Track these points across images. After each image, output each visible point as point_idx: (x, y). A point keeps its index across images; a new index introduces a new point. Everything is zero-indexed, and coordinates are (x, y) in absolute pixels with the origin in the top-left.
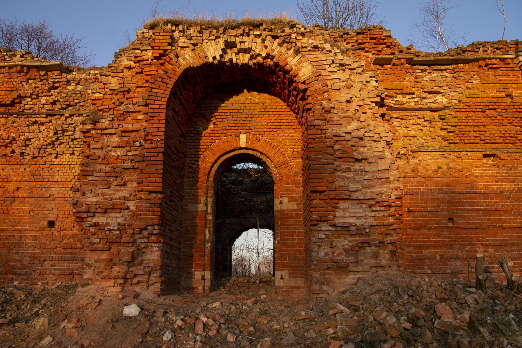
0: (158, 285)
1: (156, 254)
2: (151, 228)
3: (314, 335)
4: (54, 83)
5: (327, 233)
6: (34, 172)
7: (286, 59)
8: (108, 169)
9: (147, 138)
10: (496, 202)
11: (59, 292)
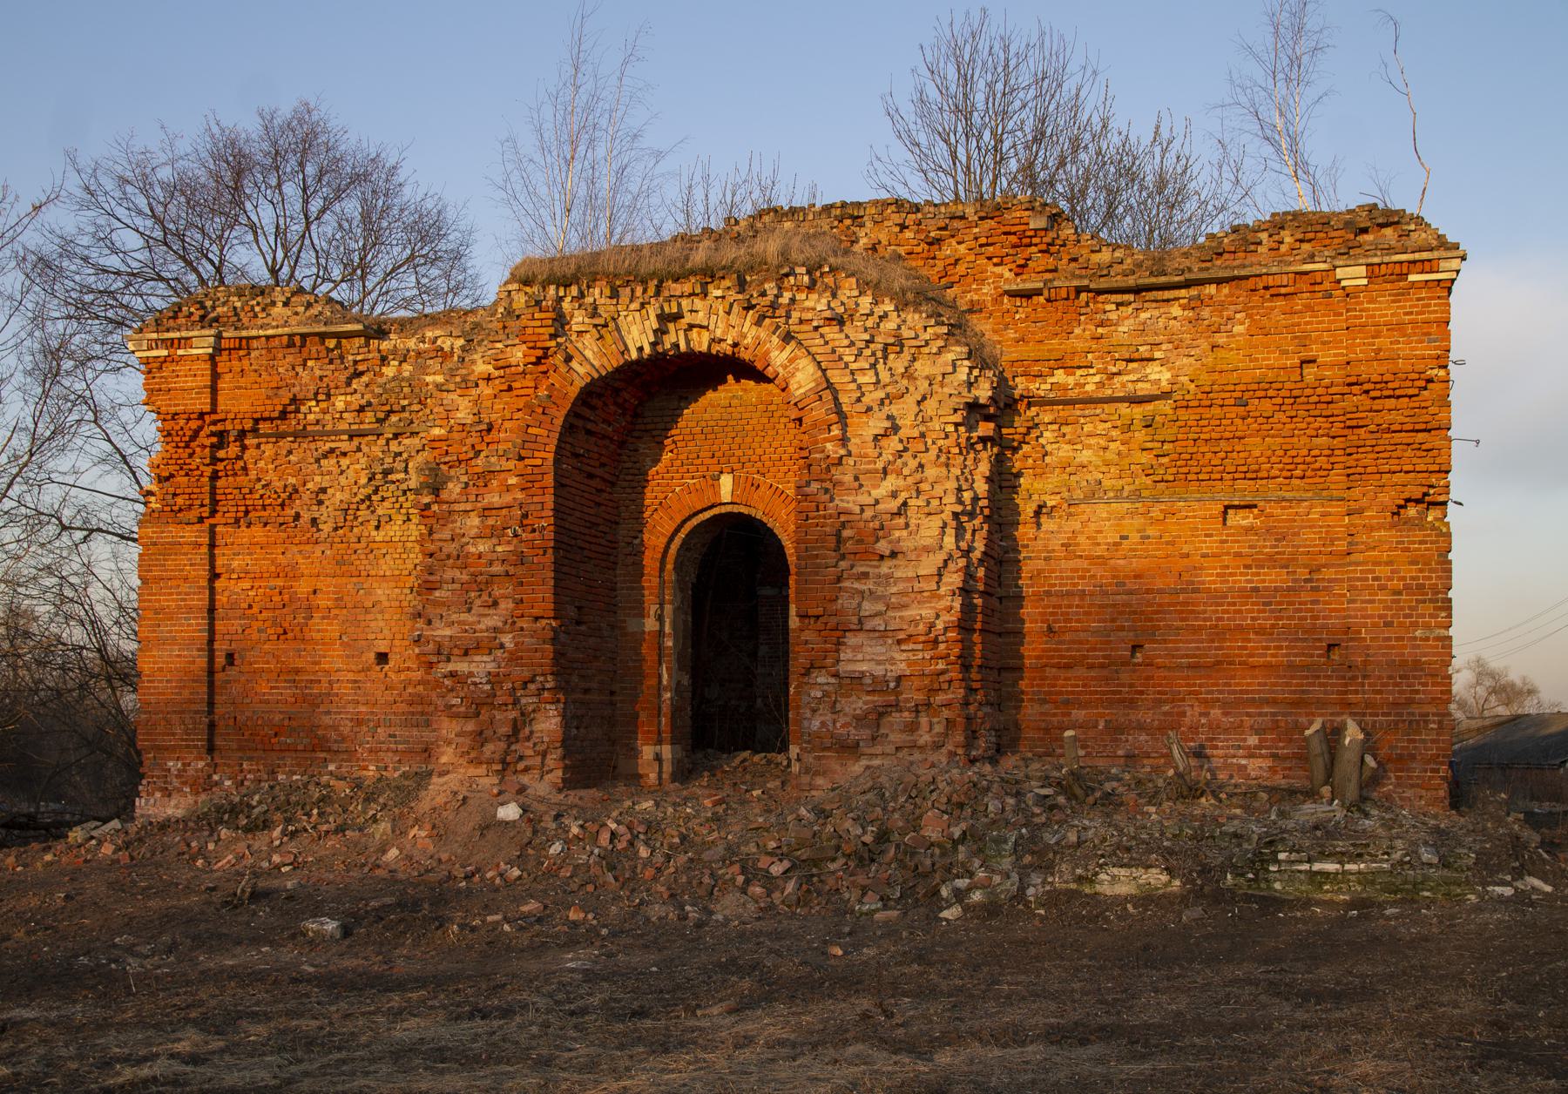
0: (560, 773)
1: (554, 721)
2: (542, 679)
3: (754, 850)
4: (356, 362)
5: (826, 688)
6: (339, 558)
7: (767, 352)
8: (465, 577)
9: (525, 522)
10: (1240, 612)
11: (406, 783)
